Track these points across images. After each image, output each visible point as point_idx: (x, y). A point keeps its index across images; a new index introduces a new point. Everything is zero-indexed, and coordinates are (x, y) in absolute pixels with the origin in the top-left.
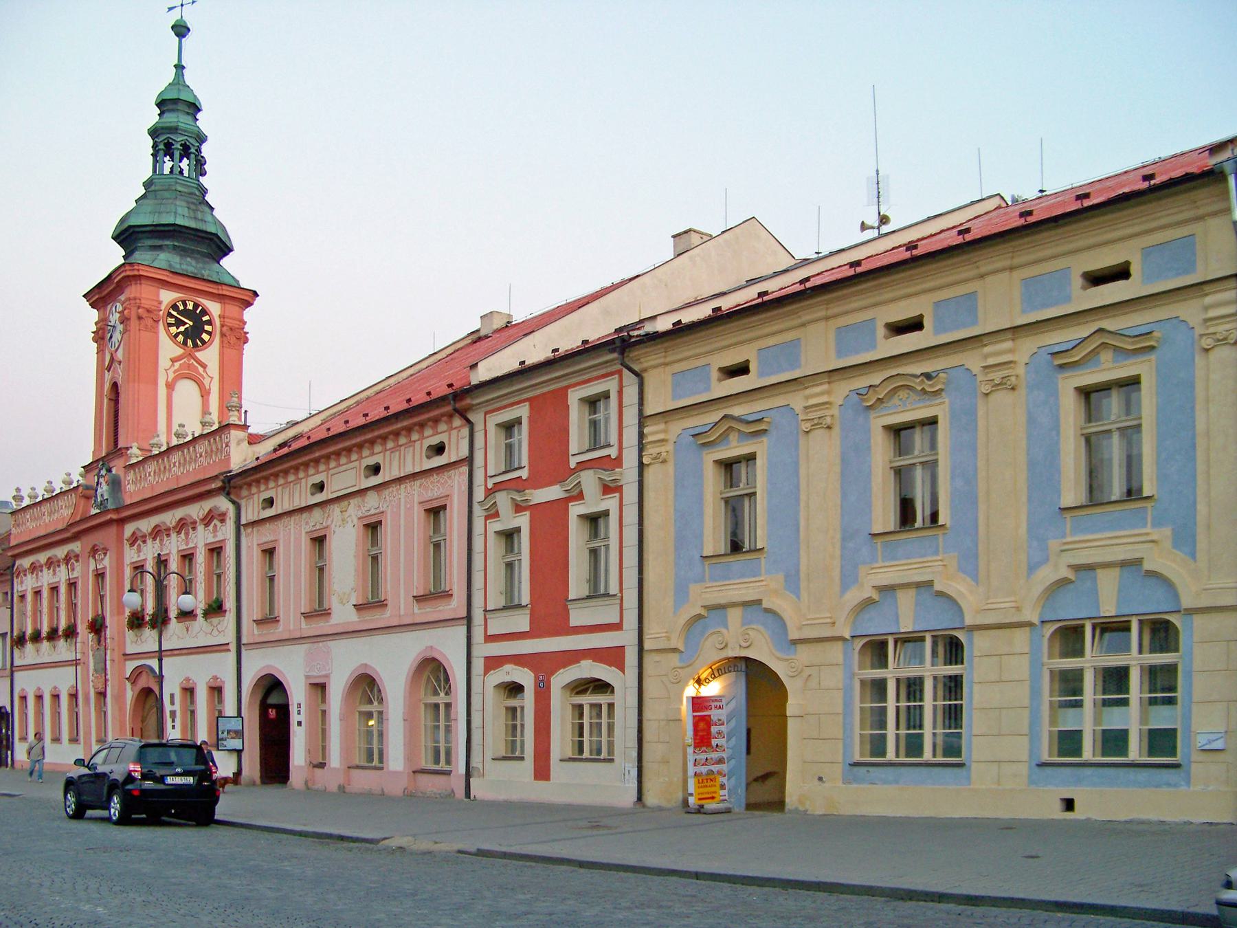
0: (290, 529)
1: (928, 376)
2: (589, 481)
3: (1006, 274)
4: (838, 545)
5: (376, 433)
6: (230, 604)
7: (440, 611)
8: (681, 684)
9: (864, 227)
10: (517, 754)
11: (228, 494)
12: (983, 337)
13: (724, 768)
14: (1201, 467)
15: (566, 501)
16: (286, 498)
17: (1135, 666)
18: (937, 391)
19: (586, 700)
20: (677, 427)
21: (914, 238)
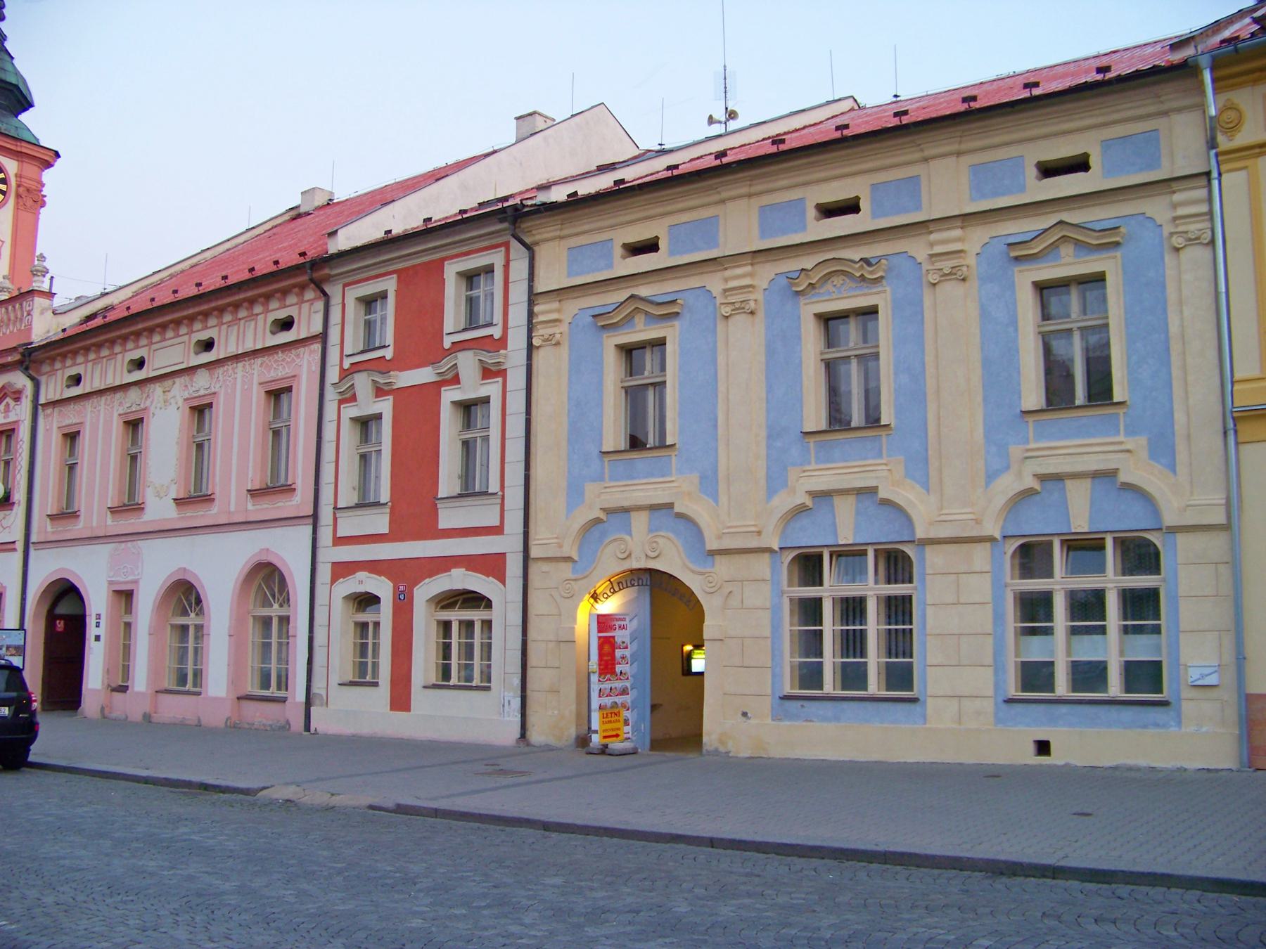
0: (99, 411)
1: (866, 261)
2: (467, 363)
3: (954, 158)
4: (764, 444)
5: (213, 304)
6: (19, 496)
7: (278, 507)
8: (573, 598)
9: (711, 121)
10: (368, 678)
11: (27, 369)
12: (928, 224)
13: (627, 699)
14: (1176, 372)
15: (437, 386)
16: (97, 374)
17: (1112, 589)
18: (875, 279)
19: (456, 616)
20: (572, 307)
21: (781, 131)
